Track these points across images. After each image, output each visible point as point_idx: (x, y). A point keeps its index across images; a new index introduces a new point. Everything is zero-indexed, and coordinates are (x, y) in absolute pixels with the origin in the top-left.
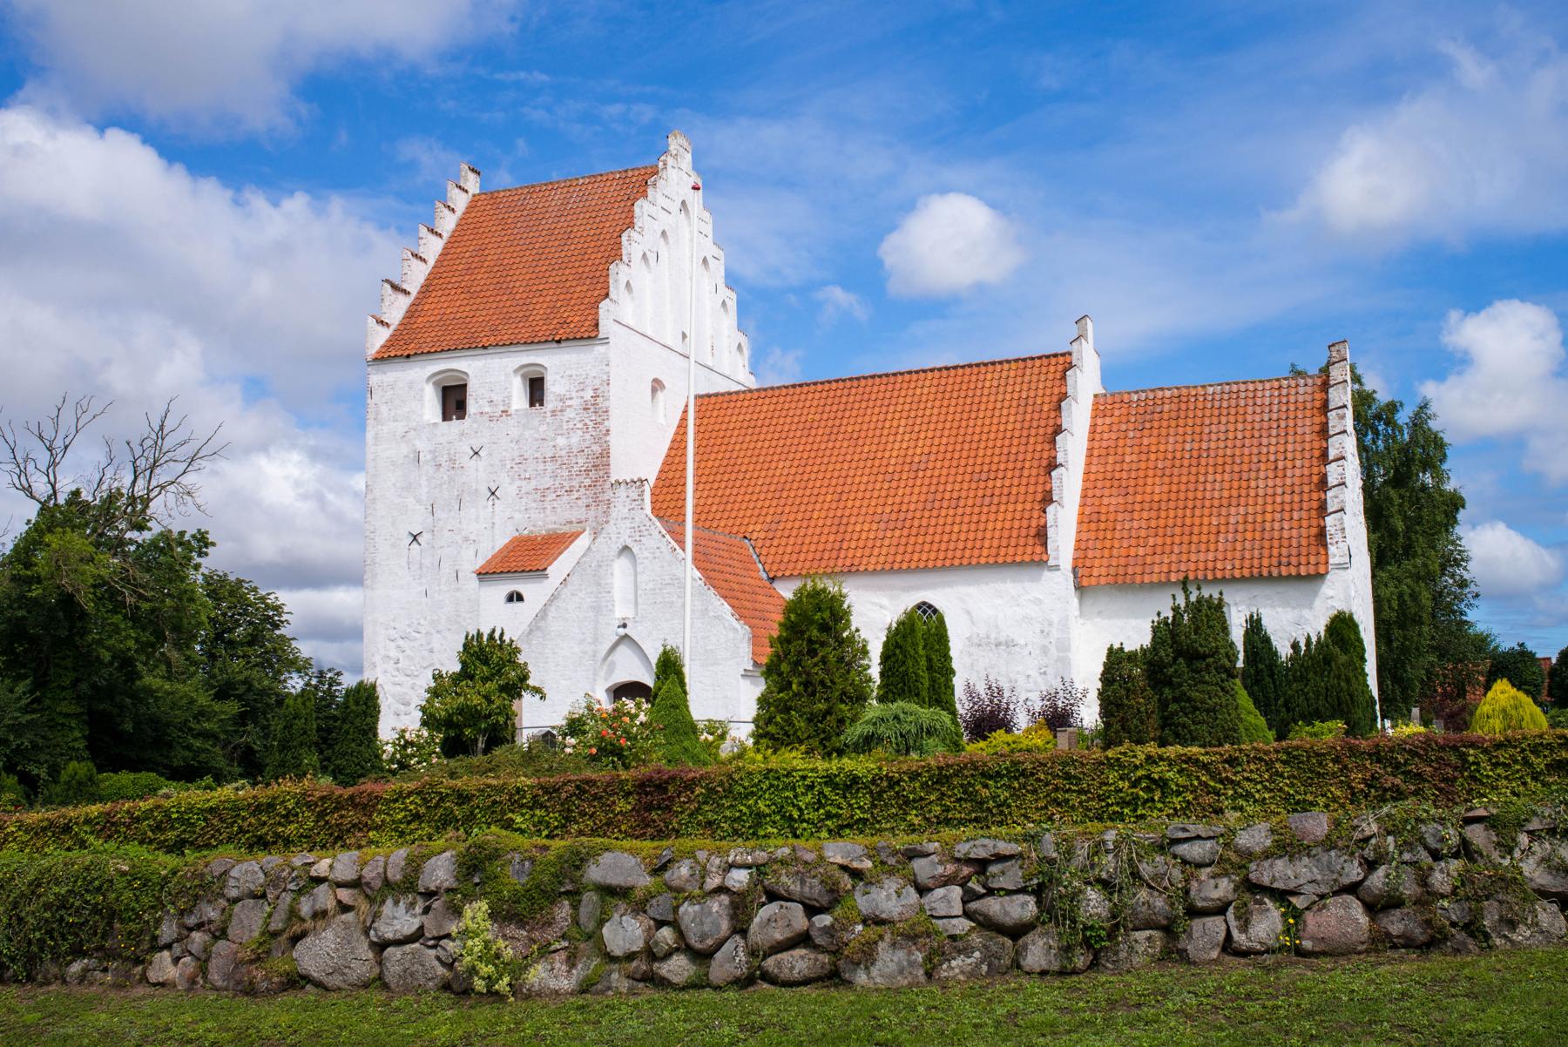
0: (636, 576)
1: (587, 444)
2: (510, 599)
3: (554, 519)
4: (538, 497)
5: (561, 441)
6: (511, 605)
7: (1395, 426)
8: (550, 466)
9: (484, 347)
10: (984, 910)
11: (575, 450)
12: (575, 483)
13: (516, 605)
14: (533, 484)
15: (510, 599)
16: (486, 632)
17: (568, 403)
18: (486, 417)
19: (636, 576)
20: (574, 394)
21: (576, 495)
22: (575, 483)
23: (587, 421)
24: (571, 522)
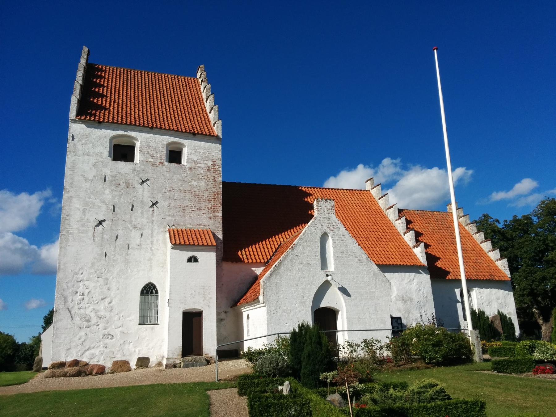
0: (70, 312)
1: (209, 187)
2: (190, 260)
3: (190, 222)
4: (181, 209)
5: (195, 183)
6: (190, 263)
7: (351, 384)
8: (188, 195)
9: (194, 134)
10: (507, 267)
11: (203, 189)
12: (203, 206)
13: (193, 264)
14: (178, 203)
15: (190, 260)
16: (44, 320)
17: (199, 165)
18: (150, 165)
19: (70, 312)
20: (202, 162)
21: (203, 212)
22: (203, 206)
23: (209, 176)
24: (200, 225)
